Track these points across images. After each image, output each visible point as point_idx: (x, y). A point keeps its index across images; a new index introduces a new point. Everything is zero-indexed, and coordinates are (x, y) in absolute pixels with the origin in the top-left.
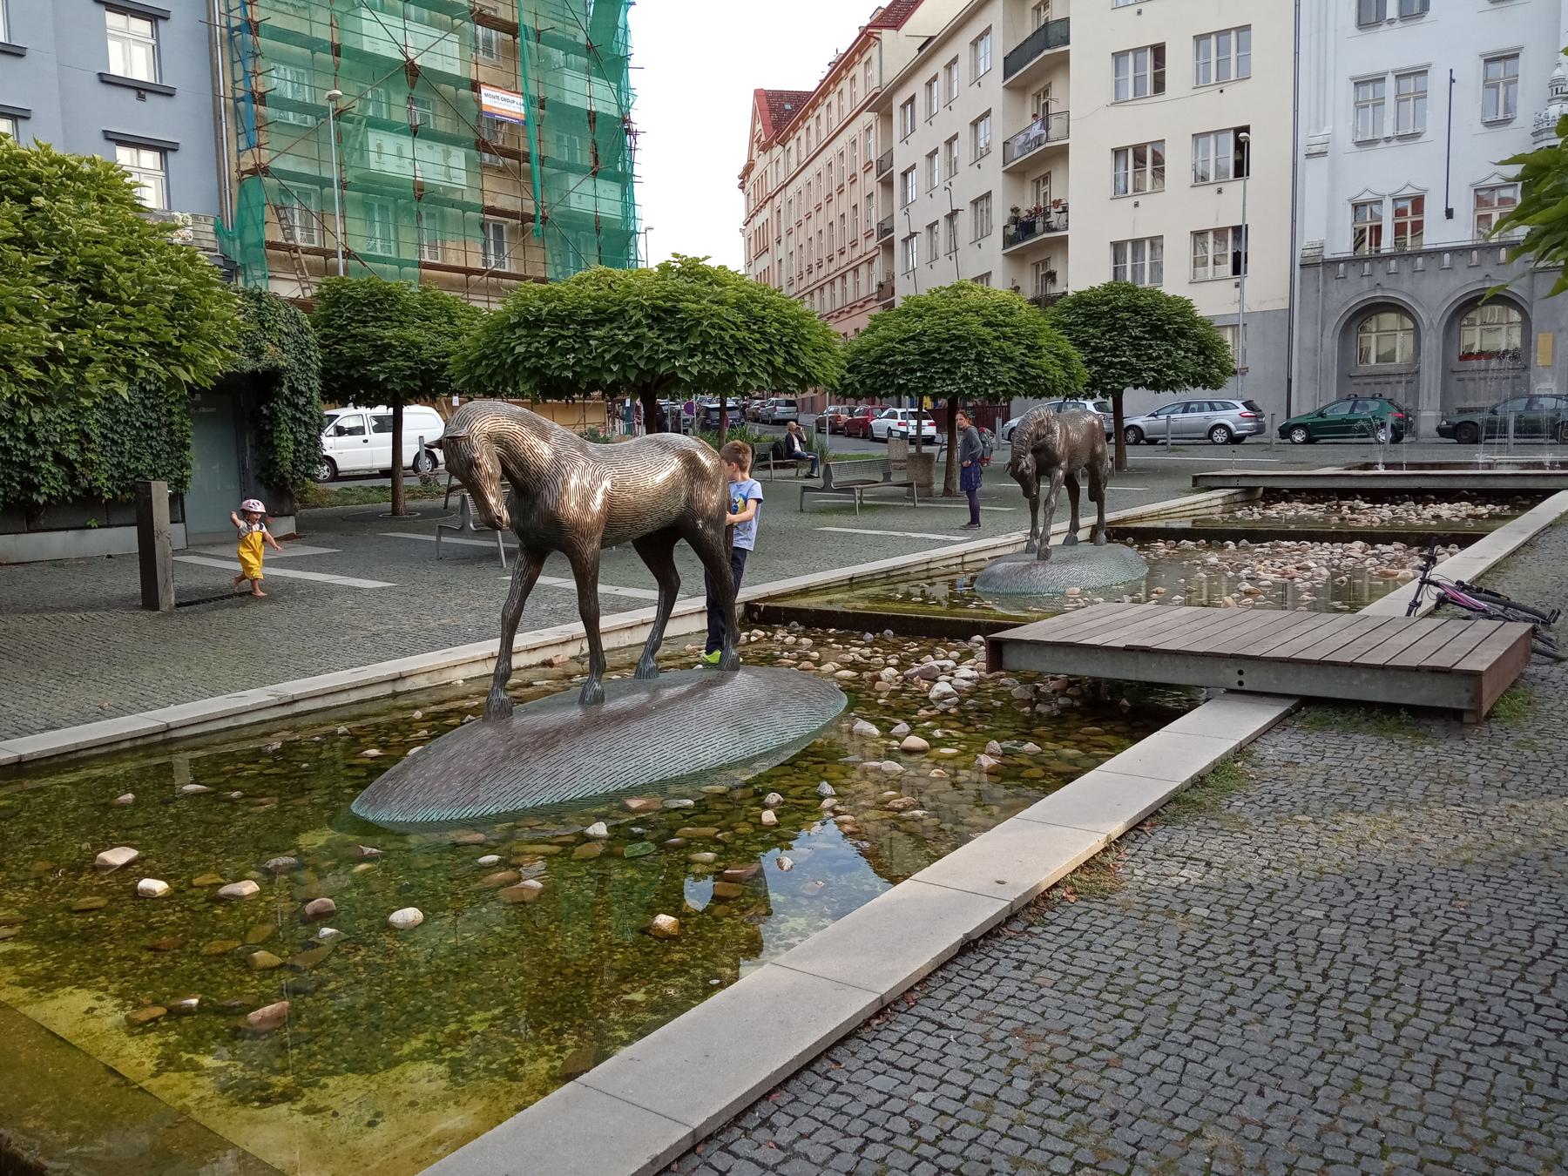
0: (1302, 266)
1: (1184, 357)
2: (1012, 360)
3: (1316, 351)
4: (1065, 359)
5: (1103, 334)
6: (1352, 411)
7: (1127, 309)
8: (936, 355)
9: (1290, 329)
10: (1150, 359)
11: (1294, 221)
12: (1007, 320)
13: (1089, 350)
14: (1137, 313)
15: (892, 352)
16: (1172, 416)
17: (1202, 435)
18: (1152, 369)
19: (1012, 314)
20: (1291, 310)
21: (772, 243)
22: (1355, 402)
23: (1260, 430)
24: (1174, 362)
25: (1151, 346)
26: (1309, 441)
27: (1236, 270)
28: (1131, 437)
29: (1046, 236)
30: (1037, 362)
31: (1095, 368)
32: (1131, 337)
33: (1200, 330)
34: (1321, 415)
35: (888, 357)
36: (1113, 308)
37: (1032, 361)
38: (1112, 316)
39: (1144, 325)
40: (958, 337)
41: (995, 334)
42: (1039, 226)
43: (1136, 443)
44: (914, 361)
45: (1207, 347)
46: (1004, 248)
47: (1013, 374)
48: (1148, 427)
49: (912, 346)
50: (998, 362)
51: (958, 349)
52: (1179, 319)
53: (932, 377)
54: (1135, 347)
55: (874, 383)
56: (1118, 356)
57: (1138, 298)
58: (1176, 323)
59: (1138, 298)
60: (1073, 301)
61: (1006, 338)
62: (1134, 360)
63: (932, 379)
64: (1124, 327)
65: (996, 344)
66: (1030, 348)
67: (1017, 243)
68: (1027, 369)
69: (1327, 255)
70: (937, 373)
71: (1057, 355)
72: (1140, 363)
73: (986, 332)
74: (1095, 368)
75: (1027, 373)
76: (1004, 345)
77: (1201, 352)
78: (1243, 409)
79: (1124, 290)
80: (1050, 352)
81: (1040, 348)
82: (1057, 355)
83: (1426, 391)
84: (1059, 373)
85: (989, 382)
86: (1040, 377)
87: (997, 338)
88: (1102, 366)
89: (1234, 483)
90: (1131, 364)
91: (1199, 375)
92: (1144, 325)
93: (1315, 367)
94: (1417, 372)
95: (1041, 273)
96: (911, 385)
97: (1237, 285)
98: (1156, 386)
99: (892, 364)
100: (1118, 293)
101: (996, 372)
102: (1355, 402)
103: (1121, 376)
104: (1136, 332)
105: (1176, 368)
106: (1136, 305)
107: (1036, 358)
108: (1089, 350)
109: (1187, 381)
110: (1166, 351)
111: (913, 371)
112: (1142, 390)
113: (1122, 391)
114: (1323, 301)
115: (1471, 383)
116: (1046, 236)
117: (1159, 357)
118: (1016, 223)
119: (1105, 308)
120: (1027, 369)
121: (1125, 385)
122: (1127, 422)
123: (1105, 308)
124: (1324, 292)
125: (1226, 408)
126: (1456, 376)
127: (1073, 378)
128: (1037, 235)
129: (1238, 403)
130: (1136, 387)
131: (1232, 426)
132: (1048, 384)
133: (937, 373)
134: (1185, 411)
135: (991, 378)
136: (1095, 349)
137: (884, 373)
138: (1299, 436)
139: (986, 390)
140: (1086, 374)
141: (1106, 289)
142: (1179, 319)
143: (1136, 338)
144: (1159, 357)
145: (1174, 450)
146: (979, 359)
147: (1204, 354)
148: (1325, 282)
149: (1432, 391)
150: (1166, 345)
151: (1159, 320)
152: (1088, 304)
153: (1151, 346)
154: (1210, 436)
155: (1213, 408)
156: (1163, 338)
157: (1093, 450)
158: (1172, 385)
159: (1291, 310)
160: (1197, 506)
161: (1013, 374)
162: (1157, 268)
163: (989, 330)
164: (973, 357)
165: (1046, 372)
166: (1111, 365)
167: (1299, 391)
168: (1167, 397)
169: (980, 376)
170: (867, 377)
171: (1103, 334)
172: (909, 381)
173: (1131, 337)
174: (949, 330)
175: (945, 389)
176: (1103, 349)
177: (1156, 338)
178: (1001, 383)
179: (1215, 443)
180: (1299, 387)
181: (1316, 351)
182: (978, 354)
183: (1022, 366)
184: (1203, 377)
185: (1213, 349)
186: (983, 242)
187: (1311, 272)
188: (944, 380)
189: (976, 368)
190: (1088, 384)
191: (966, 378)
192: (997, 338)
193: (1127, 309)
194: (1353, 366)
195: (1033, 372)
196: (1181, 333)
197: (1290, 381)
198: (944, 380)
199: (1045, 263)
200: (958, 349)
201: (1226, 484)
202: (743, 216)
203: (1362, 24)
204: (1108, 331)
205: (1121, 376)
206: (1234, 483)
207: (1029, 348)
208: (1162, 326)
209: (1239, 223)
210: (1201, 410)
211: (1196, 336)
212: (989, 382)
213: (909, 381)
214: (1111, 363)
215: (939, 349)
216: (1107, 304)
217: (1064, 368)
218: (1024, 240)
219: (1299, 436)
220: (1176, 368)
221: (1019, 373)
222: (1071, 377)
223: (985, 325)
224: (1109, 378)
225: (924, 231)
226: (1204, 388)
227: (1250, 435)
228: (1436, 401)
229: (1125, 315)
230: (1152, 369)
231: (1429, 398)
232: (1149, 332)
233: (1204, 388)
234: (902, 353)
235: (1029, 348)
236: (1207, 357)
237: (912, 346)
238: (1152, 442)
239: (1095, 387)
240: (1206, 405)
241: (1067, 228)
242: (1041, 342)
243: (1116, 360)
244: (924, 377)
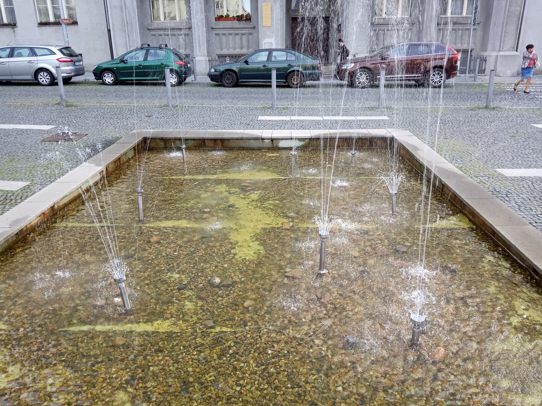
3: (121, 8)
6: (145, 59)
22: (147, 51)
26: (117, 83)
78: (59, 55)
83: (197, 41)
93: (123, 21)
94: (190, 28)
102: (147, 51)
115: (224, 36)
126: (214, 32)
129: (55, 50)
131: (53, 70)
134: (11, 55)
149: (201, 42)
181: (121, 8)
194: (149, 21)
197: (109, 31)
203: (292, 18)
219: (109, 78)
228: (204, 49)
231: (200, 46)
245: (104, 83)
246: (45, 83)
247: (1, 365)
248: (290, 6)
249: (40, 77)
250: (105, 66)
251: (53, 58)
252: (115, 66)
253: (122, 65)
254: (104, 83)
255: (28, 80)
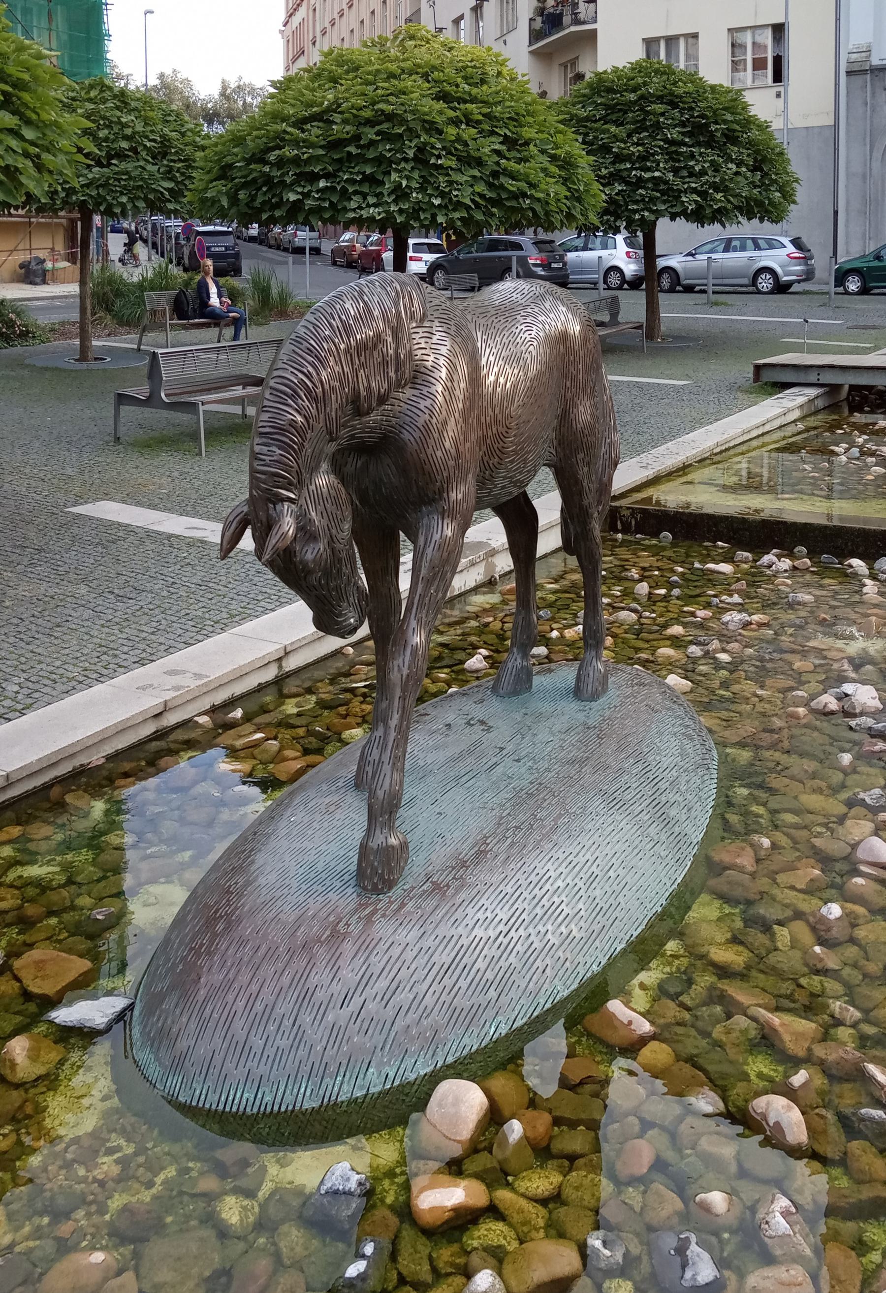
0: (849, 73)
1: (737, 173)
2: (479, 163)
4: (566, 164)
5: (629, 136)
7: (660, 99)
8: (352, 149)
9: (836, 150)
10: (691, 174)
11: (838, 19)
12: (475, 91)
13: (610, 159)
14: (673, 105)
15: (280, 140)
16: (714, 256)
17: (745, 281)
18: (694, 191)
19: (483, 82)
20: (836, 126)
21: (308, 46)
23: (809, 275)
24: (723, 180)
25: (692, 156)
26: (864, 291)
27: (778, 77)
28: (666, 282)
29: (573, 29)
30: (520, 167)
31: (618, 187)
32: (666, 140)
33: (754, 134)
34: (878, 258)
35: (273, 149)
36: (642, 97)
37: (513, 166)
38: (642, 109)
39: (683, 124)
40: (390, 117)
41: (452, 114)
42: (567, 19)
43: (672, 290)
44: (312, 159)
45: (764, 160)
46: (530, 44)
47: (480, 188)
48: (685, 269)
49: (316, 131)
50: (453, 163)
51: (387, 137)
52: (729, 117)
53: (344, 191)
54: (673, 157)
55: (253, 198)
56: (649, 169)
57: (675, 84)
58: (725, 122)
59: (675, 84)
60: (590, 85)
61: (469, 122)
62: (670, 176)
63: (345, 195)
64: (657, 126)
65: (451, 131)
66: (510, 142)
67: (542, 39)
68: (504, 180)
69: (875, 61)
70: (353, 182)
71: (554, 158)
72: (678, 181)
73: (434, 109)
74: (618, 187)
75: (502, 187)
76: (465, 136)
77: (755, 169)
78: (791, 248)
79: (657, 71)
80: (543, 152)
81: (527, 143)
82: (554, 158)
84: (554, 189)
85: (437, 202)
86: (524, 195)
87: (456, 122)
88: (627, 183)
89: (812, 378)
90: (666, 182)
91: (755, 200)
92: (683, 124)
95: (570, 76)
96: (309, 203)
97: (778, 95)
98: (699, 216)
99: (280, 163)
100: (648, 75)
101: (450, 183)
103: (652, 200)
104: (674, 134)
105: (726, 190)
106: (672, 94)
107: (519, 161)
108: (610, 159)
109: (739, 208)
110: (712, 162)
111: (314, 178)
112: (681, 222)
113: (654, 224)
114: (871, 117)
116: (573, 29)
117: (703, 172)
118: (542, 15)
119: (632, 97)
120: (504, 180)
121: (658, 214)
122: (661, 263)
123: (632, 97)
124: (872, 104)
125: (771, 247)
127: (579, 200)
128: (564, 29)
130: (673, 218)
131: (779, 270)
132: (538, 207)
133: (353, 182)
134: (726, 250)
135: (442, 194)
136: (619, 158)
137: (268, 180)
138: (853, 285)
139: (434, 216)
140: (599, 196)
141: (633, 69)
142: (729, 117)
143: (672, 142)
144: (703, 172)
145: (716, 304)
146: (421, 158)
147: (761, 170)
148: (873, 94)
150: (712, 155)
151: (703, 116)
152: (610, 90)
153: (692, 156)
154: (754, 282)
155: (757, 247)
156: (708, 145)
157: (565, 418)
158: (719, 216)
159: (836, 126)
160: (767, 428)
161: (480, 188)
162: (692, 56)
163: (441, 105)
164: (411, 154)
165: (532, 185)
166: (640, 183)
167: (847, 226)
168: (713, 231)
169: (422, 189)
170: (244, 186)
171: (629, 136)
172: (307, 195)
173: (666, 140)
174: (374, 104)
175: (365, 214)
176: (628, 158)
177: (698, 144)
178: (459, 205)
179: (759, 292)
180: (847, 221)
181: (864, 177)
182: (421, 149)
183: (495, 174)
184: (760, 204)
185: (771, 161)
186: (508, 38)
187: (858, 80)
188: (364, 196)
189: (416, 175)
190: (606, 212)
191: (400, 194)
192: (456, 122)
193: (660, 99)
195: (511, 185)
196: (731, 137)
197: (836, 213)
198: (364, 196)
199: (574, 62)
200: (387, 137)
201: (802, 378)
202: (282, 16)
203: (729, 30)
204: (637, 131)
205: (652, 200)
206: (812, 378)
207: (506, 140)
208: (707, 125)
209: (780, 20)
210: (743, 248)
211: (751, 144)
212: (437, 202)
213: (307, 195)
214: (640, 179)
215: (356, 138)
216: (634, 90)
217: (565, 181)
218: (550, 34)
219: (853, 285)
220: (726, 190)
221: (491, 186)
222: (577, 197)
223: (437, 98)
224: (636, 202)
225: (450, 26)
226: (762, 220)
227: (799, 282)
229: (659, 108)
230: (694, 191)
232: (690, 134)
233: (762, 220)
234: (296, 143)
235: (506, 140)
236: (765, 175)
237: (316, 131)
238: (689, 289)
239: (618, 217)
240: (750, 243)
241: (595, 21)
242: (528, 133)
243: (647, 175)
244: (333, 189)
245: (847, 293)
246: (765, 289)
247: (882, 423)
248: (870, 348)
249: (760, 280)
250: (848, 266)
251: (783, 252)
252: (866, 265)
253: (876, 263)
254: (847, 293)
255: (742, 286)
